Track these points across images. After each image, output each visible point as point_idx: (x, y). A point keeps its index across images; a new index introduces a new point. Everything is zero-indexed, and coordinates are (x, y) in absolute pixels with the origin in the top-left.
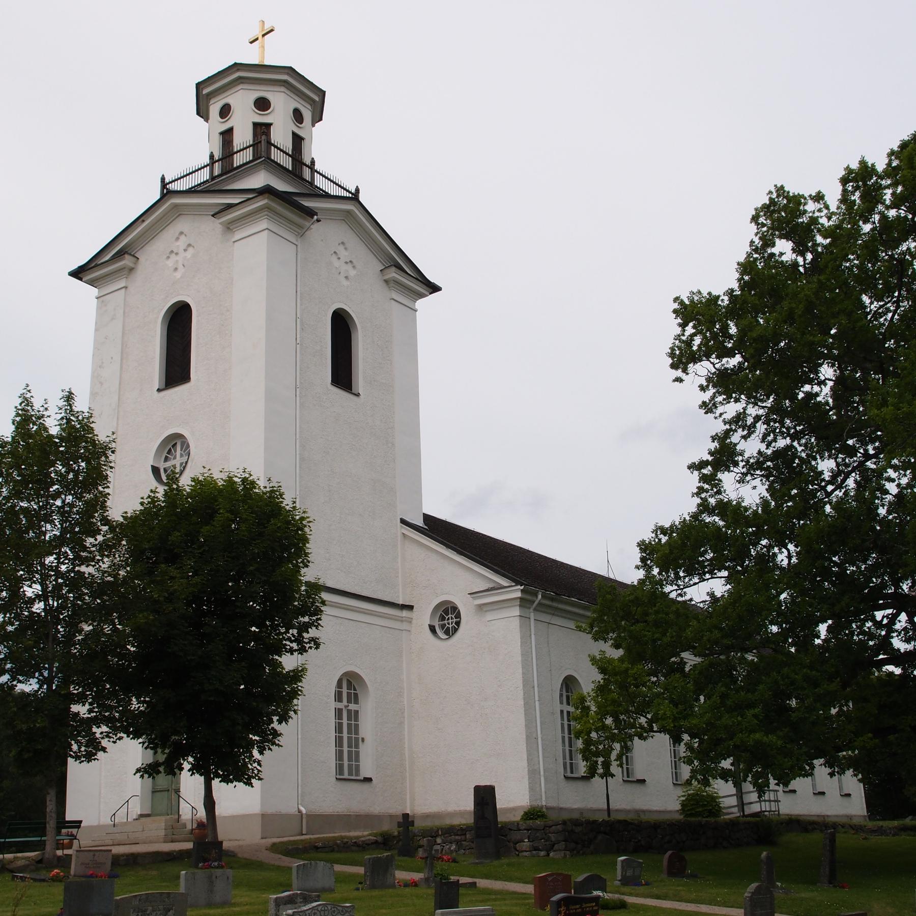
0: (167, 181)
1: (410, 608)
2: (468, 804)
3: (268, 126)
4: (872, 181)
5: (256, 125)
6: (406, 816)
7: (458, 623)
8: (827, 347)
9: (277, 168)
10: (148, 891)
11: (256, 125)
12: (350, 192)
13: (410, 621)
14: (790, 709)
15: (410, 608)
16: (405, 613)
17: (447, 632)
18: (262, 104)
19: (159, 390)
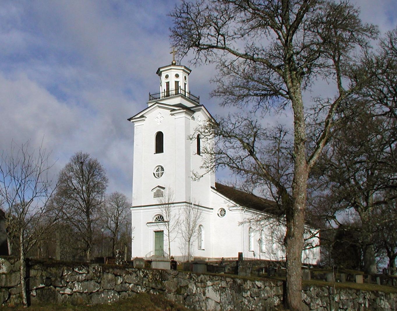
0: (151, 94)
1: (212, 209)
2: (237, 256)
3: (178, 82)
4: (348, 241)
5: (176, 82)
6: (223, 258)
7: (225, 214)
8: (325, 31)
9: (184, 97)
10: (20, 252)
11: (176, 82)
12: (197, 98)
13: (212, 212)
14: (284, 215)
15: (212, 209)
16: (211, 210)
17: (222, 215)
18: (177, 76)
19: (154, 154)
